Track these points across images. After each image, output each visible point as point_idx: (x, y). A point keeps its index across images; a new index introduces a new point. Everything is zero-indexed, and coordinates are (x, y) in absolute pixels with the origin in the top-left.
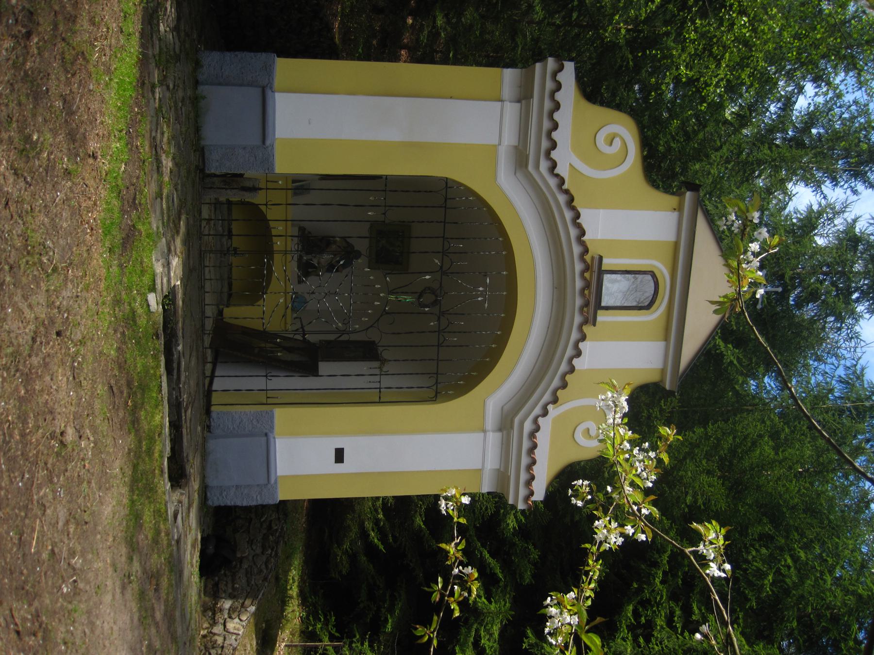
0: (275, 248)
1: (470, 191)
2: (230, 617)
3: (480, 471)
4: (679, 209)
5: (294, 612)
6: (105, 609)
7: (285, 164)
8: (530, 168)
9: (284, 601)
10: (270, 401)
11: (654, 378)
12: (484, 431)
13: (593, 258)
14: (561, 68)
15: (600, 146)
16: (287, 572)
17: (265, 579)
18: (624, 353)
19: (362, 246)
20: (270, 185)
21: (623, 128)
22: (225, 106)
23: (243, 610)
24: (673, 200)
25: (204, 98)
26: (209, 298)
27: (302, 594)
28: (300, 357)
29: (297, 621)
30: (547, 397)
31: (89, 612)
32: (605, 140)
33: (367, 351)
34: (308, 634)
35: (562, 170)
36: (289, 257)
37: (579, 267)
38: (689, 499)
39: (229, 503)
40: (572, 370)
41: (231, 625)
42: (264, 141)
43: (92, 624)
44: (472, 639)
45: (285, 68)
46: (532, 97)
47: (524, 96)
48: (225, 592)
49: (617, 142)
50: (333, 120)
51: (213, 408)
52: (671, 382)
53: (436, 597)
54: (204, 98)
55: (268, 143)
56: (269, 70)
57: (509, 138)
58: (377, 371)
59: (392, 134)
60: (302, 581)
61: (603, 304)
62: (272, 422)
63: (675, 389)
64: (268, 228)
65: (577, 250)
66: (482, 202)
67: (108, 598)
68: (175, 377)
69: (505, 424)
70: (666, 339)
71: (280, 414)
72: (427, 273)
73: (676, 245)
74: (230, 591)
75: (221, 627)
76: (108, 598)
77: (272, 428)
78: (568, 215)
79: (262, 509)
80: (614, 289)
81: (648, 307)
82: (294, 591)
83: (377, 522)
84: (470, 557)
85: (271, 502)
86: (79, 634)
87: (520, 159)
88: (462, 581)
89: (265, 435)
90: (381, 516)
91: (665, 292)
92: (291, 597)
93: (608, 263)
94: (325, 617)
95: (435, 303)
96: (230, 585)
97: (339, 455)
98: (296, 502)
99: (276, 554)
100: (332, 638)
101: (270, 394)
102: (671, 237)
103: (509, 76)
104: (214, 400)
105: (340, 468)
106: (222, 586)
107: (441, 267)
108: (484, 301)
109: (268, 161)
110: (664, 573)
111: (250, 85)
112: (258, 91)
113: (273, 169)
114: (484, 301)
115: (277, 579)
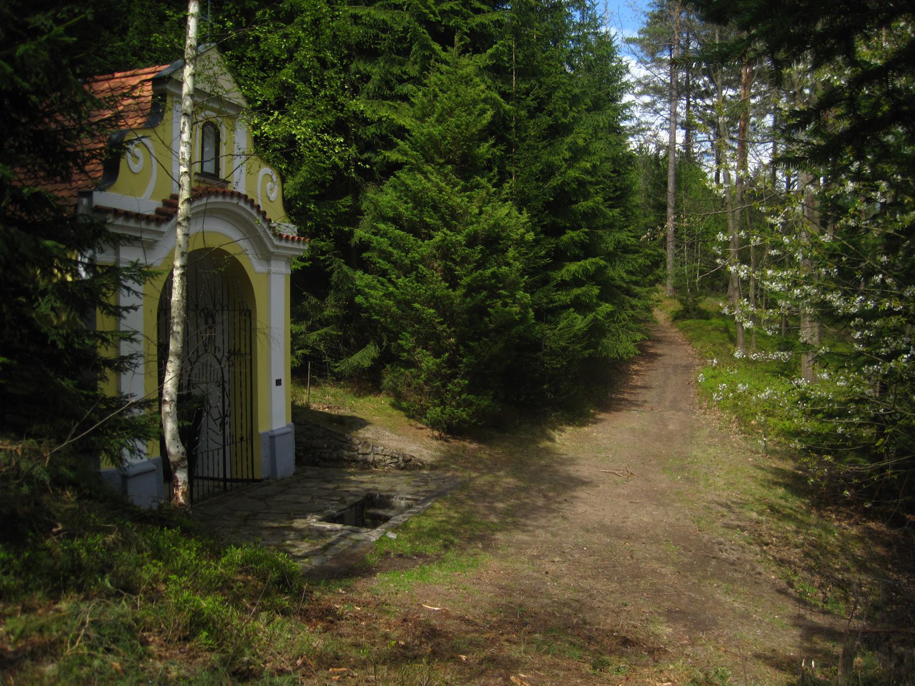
74: (330, 450)
77: (267, 433)
105: (274, 382)
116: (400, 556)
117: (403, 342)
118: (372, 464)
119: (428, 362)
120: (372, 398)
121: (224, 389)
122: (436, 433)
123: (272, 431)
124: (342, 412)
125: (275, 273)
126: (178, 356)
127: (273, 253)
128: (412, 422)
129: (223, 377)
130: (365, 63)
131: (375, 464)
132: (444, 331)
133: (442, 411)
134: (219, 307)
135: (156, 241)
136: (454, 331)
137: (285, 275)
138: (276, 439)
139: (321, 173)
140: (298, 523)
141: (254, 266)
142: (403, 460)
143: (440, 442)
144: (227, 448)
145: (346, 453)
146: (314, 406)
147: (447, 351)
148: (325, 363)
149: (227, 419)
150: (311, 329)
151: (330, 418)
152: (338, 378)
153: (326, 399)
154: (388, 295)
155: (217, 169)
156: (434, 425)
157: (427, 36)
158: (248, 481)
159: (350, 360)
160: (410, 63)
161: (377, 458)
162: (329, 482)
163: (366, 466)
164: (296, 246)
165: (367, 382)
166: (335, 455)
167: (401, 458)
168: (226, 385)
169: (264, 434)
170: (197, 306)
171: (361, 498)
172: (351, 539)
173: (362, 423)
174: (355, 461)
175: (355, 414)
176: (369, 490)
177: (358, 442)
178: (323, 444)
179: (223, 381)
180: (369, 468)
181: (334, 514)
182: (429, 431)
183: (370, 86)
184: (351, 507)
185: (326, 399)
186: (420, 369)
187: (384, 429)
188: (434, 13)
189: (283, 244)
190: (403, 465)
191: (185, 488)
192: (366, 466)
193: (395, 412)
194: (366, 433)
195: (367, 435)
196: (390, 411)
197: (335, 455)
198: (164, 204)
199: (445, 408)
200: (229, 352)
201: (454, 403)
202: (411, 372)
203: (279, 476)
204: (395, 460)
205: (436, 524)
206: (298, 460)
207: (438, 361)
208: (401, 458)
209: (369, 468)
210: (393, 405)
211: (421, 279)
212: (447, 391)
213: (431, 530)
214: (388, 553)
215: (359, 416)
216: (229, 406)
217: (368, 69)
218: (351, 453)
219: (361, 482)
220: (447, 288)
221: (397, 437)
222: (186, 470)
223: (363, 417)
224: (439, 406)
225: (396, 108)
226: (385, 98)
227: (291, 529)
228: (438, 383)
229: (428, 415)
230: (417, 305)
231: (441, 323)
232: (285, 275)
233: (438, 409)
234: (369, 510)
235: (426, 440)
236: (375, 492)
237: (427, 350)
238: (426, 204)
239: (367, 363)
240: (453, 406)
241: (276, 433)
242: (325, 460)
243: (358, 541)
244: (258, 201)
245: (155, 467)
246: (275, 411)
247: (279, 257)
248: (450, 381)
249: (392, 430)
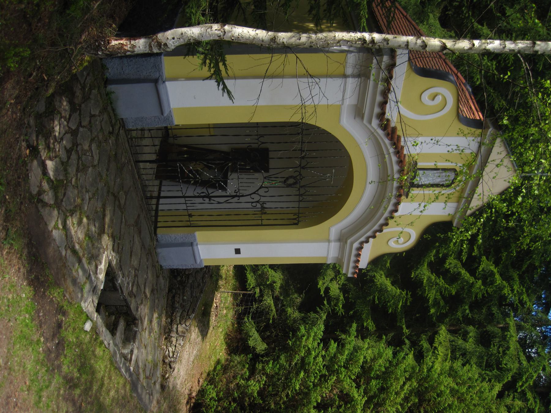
2: (180, 323)
11: (448, 219)
21: (452, 99)
23: (188, 317)
32: (429, 99)
40: (392, 218)
48: (178, 302)
57: (350, 100)
68: (120, 291)
69: (342, 239)
74: (181, 301)
77: (195, 240)
81: (448, 186)
91: (462, 177)
93: (420, 165)
96: (181, 297)
101: (192, 222)
105: (237, 247)
107: (300, 165)
116: (59, 325)
117: (270, 365)
118: (169, 335)
119: (254, 387)
120: (224, 347)
121: (233, 197)
122: (194, 394)
123: (197, 245)
124: (213, 318)
125: (329, 245)
126: (273, 40)
127: (346, 242)
128: (204, 376)
129: (243, 196)
130: (475, 337)
131: (168, 339)
132: (281, 398)
133: (213, 398)
134: (302, 191)
135: (362, 118)
136: (280, 408)
137: (327, 258)
138: (190, 248)
139: (394, 303)
140: (106, 241)
141: (336, 225)
142: (171, 362)
143: (187, 396)
144: (182, 200)
145: (179, 314)
146: (218, 295)
147: (264, 402)
148: (252, 305)
149: (207, 200)
150: (276, 299)
151: (208, 306)
152: (239, 318)
153: (223, 302)
154: (309, 352)
155: (418, 186)
156: (202, 392)
157: (506, 381)
158: (156, 222)
159: (254, 329)
160: (480, 370)
161: (174, 340)
162: (152, 291)
163: (167, 332)
164: (352, 265)
165: (237, 343)
166: (177, 305)
167: (172, 359)
168: (236, 199)
169: (195, 236)
170: (303, 168)
171: (134, 313)
172: (85, 283)
173: (204, 332)
174: (171, 323)
175: (211, 328)
176: (142, 323)
177: (188, 324)
178: (186, 293)
179: (239, 196)
180: (165, 333)
181: (117, 280)
182: (196, 388)
183: (460, 342)
184: (125, 300)
185: (223, 302)
186: (248, 379)
187: (198, 351)
188: (522, 385)
189: (354, 252)
190: (167, 361)
191: (128, 48)
192: (167, 332)
193: (213, 363)
194: (195, 334)
195: (193, 333)
196: (214, 359)
197: (177, 305)
198: (393, 128)
199: (215, 401)
200: (264, 203)
201: (219, 408)
202: (246, 373)
203: (159, 250)
204: (171, 355)
205: (99, 375)
206: (175, 273)
207: (256, 394)
208: (172, 359)
209: (165, 333)
210: (218, 362)
211: (324, 378)
212: (230, 404)
213: (91, 367)
214: (64, 313)
215: (210, 331)
216: (219, 203)
217: (471, 340)
218: (178, 318)
219: (150, 321)
220: (317, 401)
221: (191, 359)
222: (147, 51)
223: (209, 335)
224: (217, 395)
225: (446, 360)
226: (453, 352)
227: (102, 231)
228: (236, 394)
229: (209, 386)
230: (302, 374)
231: (287, 396)
232: (327, 258)
233: (214, 395)
234: (118, 313)
235: (189, 385)
236: (140, 327)
237: (264, 385)
238: (385, 380)
239: (251, 343)
240: (217, 407)
241: (195, 247)
242: (173, 297)
243: (82, 290)
244: (386, 230)
245: (165, 115)
246: (217, 249)
247: (342, 250)
248: (238, 405)
249: (198, 357)
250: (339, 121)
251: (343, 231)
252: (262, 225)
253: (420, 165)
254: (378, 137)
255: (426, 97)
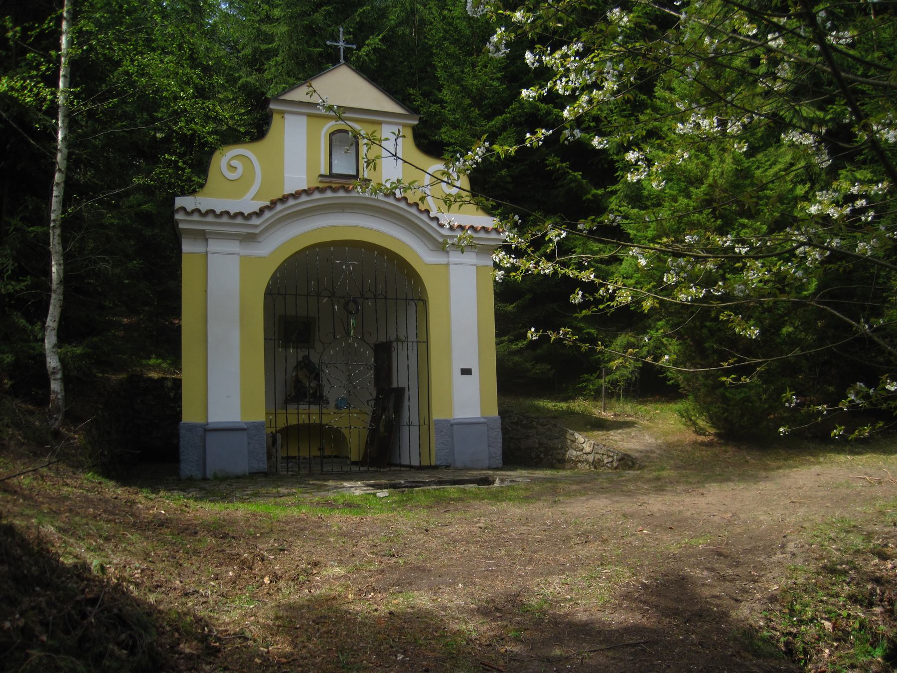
0: (318, 422)
1: (274, 277)
3: (478, 267)
4: (282, 113)
5: (579, 405)
6: (575, 510)
7: (259, 415)
8: (257, 231)
9: (571, 413)
10: (427, 423)
12: (448, 264)
13: (321, 182)
14: (184, 209)
15: (239, 177)
16: (549, 410)
17: (555, 426)
18: (394, 158)
19: (302, 353)
20: (273, 424)
22: (223, 458)
24: (276, 118)
25: (215, 474)
26: (347, 469)
27: (565, 400)
28: (390, 404)
29: (586, 403)
30: (424, 217)
31: (577, 517)
33: (384, 353)
34: (596, 395)
35: (256, 206)
36: (324, 411)
37: (329, 194)
38: (495, 83)
39: (500, 452)
41: (587, 449)
42: (244, 429)
43: (583, 516)
44: (603, 266)
45: (190, 415)
46: (204, 231)
47: (203, 236)
49: (234, 163)
50: (226, 379)
51: (433, 463)
52: (415, 120)
53: (571, 343)
54: (215, 474)
55: (245, 426)
56: (192, 427)
57: (235, 247)
58: (405, 344)
59: (235, 336)
60: (555, 399)
61: (353, 173)
62: (442, 421)
63: (418, 117)
64: (304, 425)
65: (317, 195)
66: (282, 268)
67: (569, 510)
69: (441, 247)
70: (380, 123)
71: (437, 415)
72: (333, 308)
73: (309, 115)
75: (589, 456)
76: (569, 510)
77: (447, 421)
78: (291, 202)
79: (505, 430)
80: (343, 166)
82: (564, 405)
83: (511, 342)
84: (557, 330)
85: (500, 421)
86: (588, 521)
87: (250, 238)
88: (565, 334)
89: (451, 427)
90: (506, 338)
92: (568, 407)
93: (324, 170)
94: (584, 381)
95: (355, 301)
96: (559, 451)
97: (466, 372)
98: (499, 405)
99: (537, 418)
100: (600, 377)
101: (422, 423)
102: (304, 119)
103: (188, 247)
104: (425, 463)
105: (475, 371)
106: (560, 457)
108: (353, 265)
109: (258, 426)
110: (555, 107)
111: (204, 441)
112: (208, 434)
113: (263, 423)
114: (353, 265)
115: (555, 417)
250: (264, 257)
251: (431, 248)
252: (427, 342)
253: (324, 170)
254: (281, 215)
255: (231, 176)
